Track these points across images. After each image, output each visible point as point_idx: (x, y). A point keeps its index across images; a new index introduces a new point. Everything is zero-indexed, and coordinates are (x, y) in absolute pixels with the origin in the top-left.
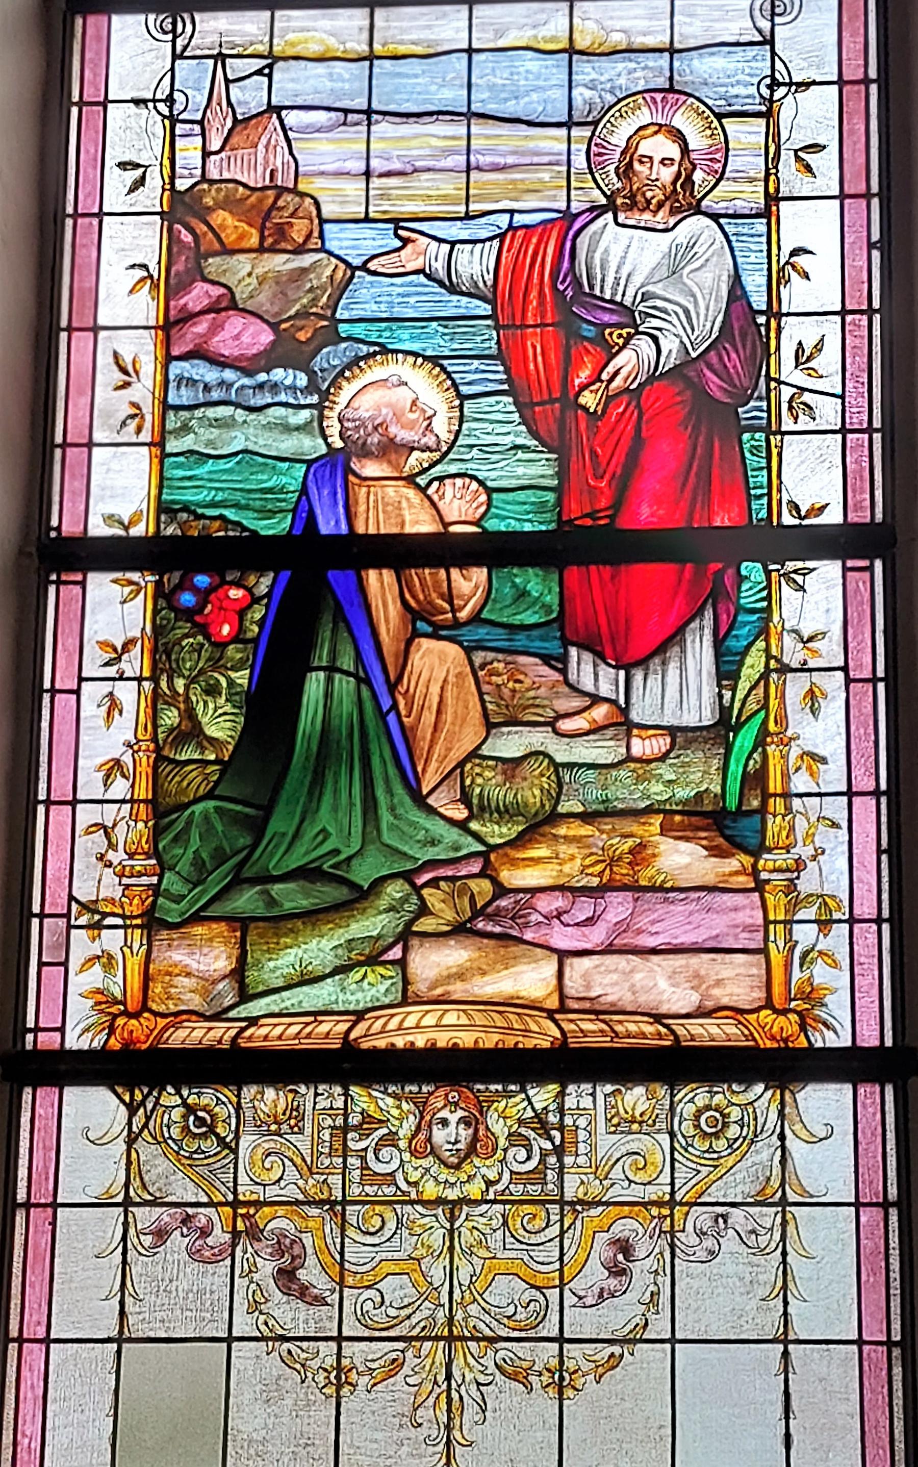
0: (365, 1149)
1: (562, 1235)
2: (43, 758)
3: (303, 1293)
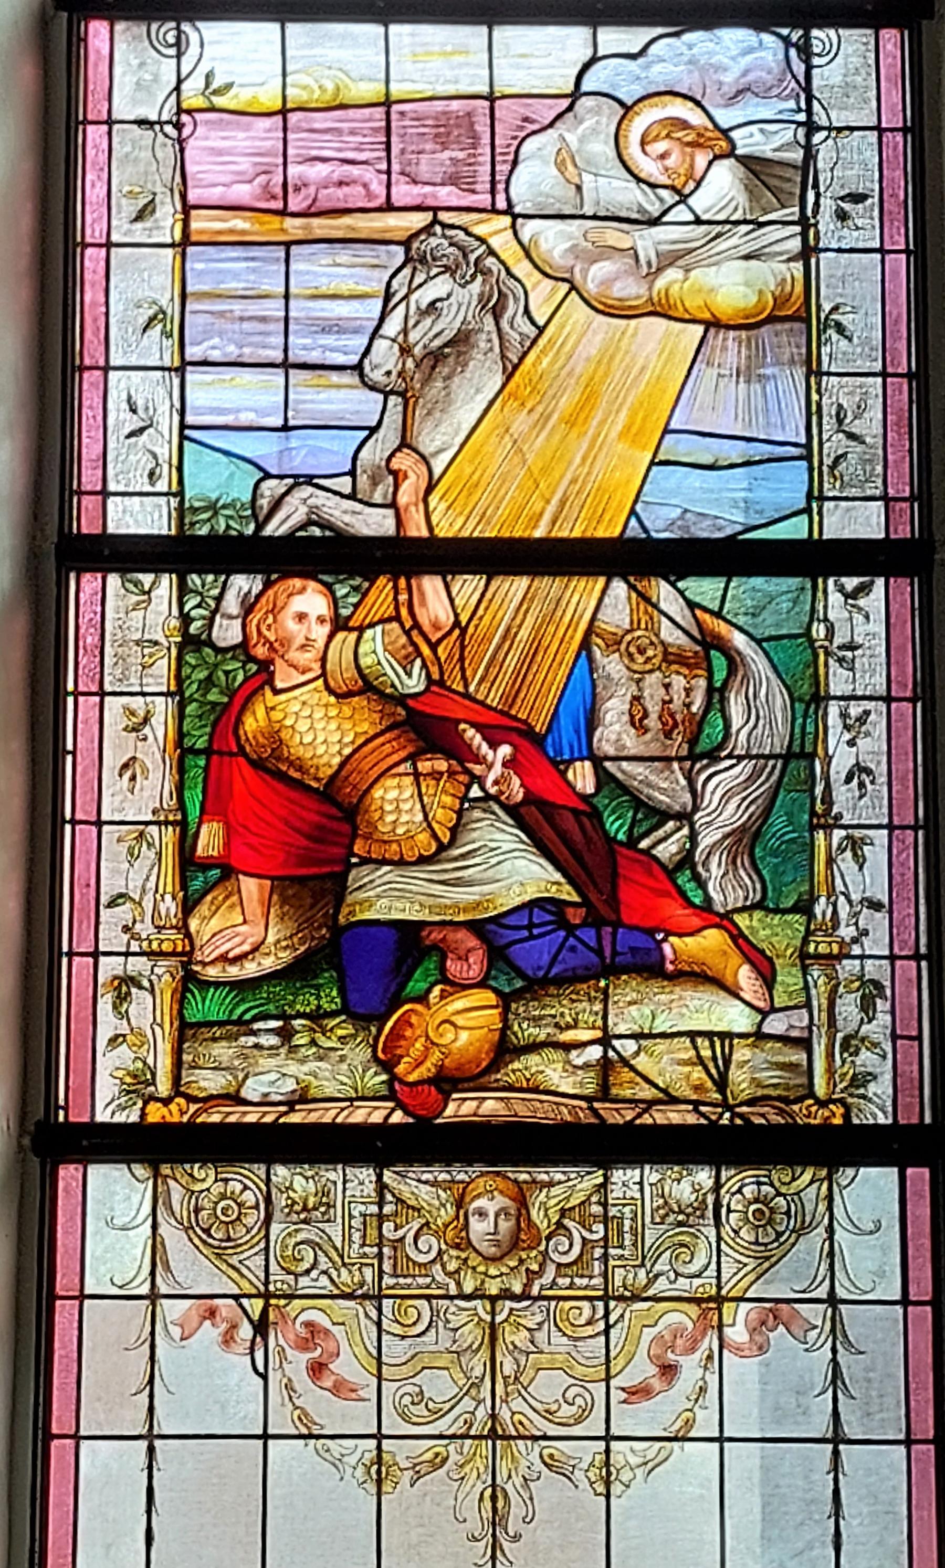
1: (606, 1332)
3: (340, 1389)
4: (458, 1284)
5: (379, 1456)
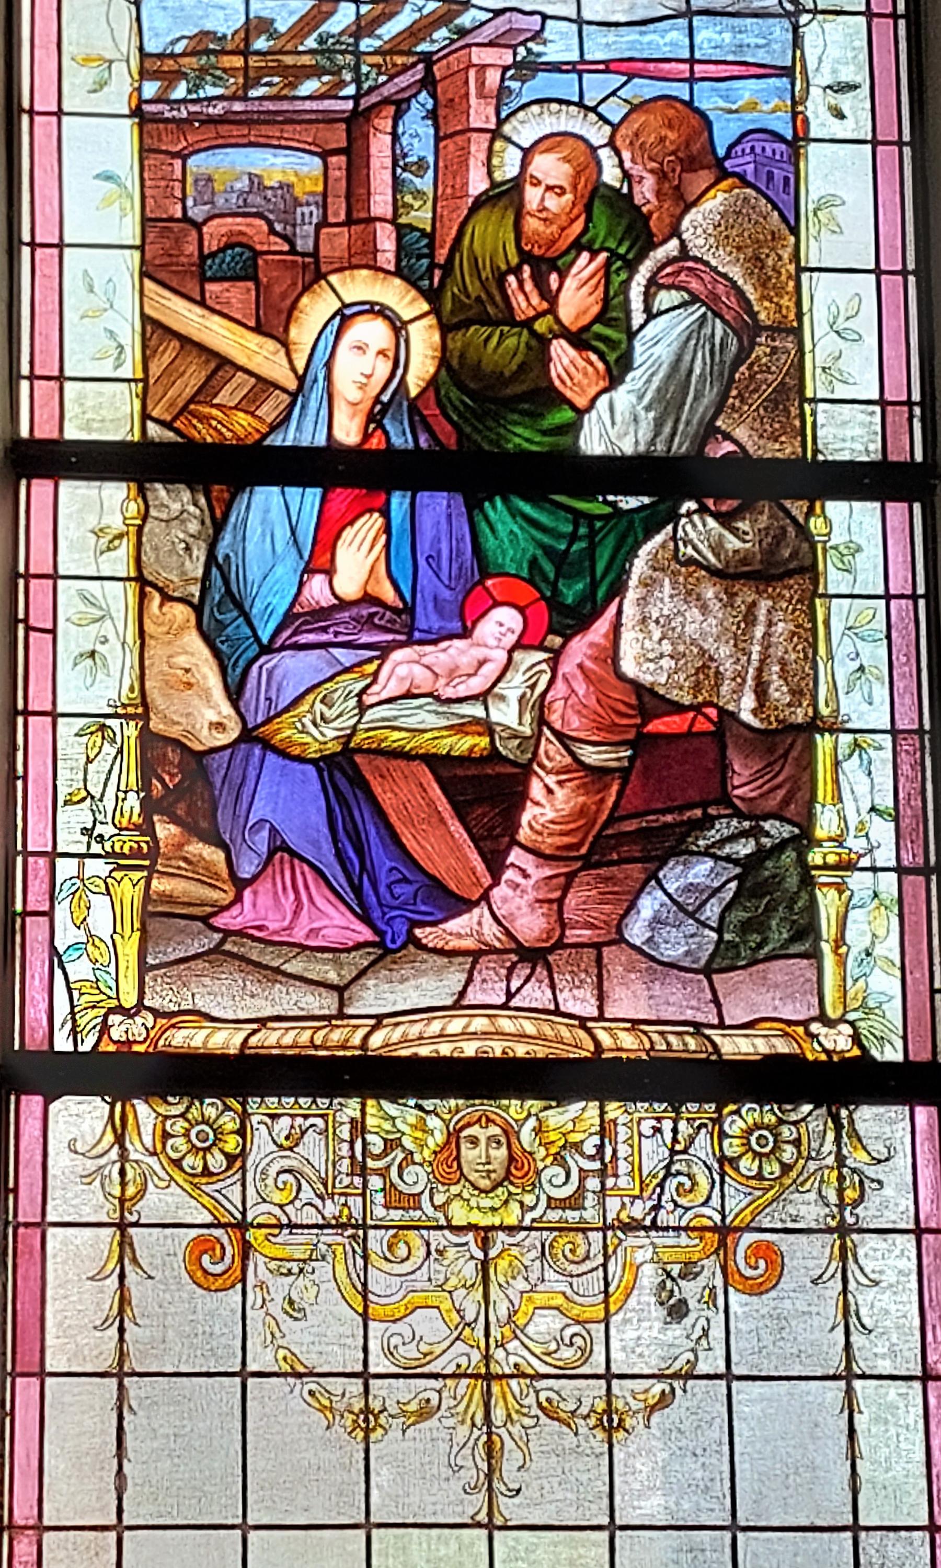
0: (388, 1168)
1: (605, 1266)
5: (366, 1439)
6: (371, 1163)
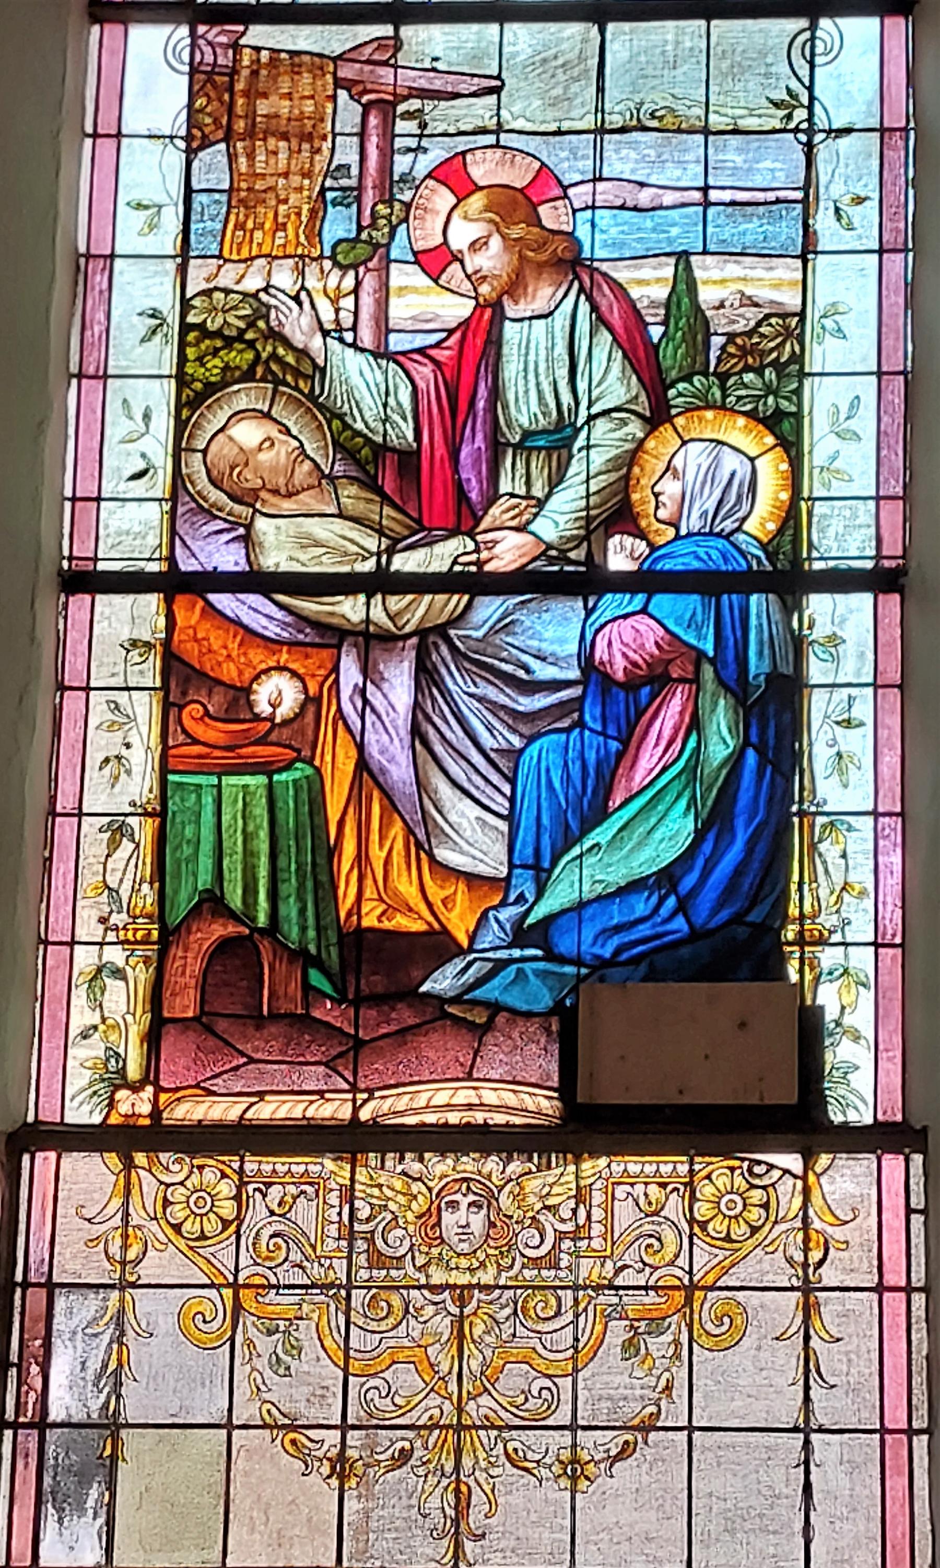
0: (372, 1232)
1: (575, 1322)
2: (22, 1227)
4: (427, 1276)
6: (357, 1227)
